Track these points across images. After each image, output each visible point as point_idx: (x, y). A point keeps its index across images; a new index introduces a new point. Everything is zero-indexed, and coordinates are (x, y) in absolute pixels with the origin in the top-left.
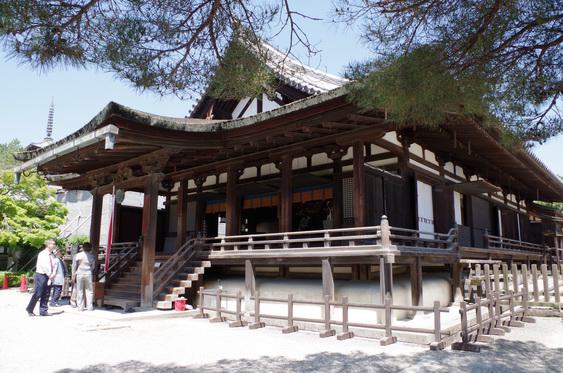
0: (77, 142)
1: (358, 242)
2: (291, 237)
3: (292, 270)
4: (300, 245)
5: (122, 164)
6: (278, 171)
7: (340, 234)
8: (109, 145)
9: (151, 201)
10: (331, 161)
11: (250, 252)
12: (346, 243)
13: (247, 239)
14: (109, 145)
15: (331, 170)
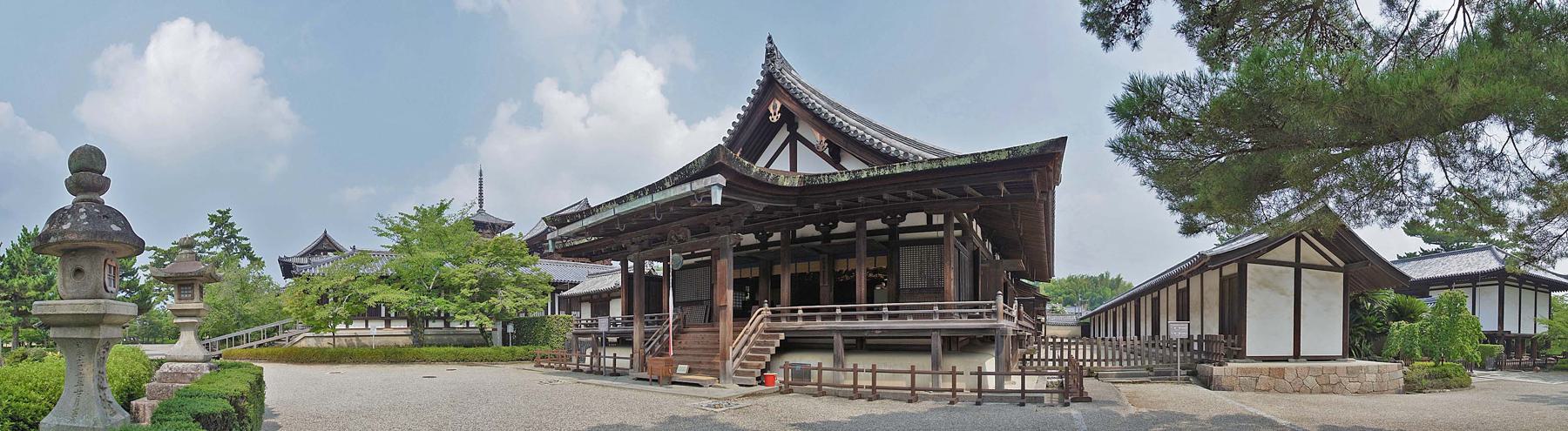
0: (659, 197)
1: (916, 316)
2: (890, 308)
3: (869, 341)
4: (814, 318)
5: (675, 224)
6: (818, 233)
7: (897, 308)
8: (717, 198)
9: (640, 266)
10: (818, 233)
11: (838, 324)
12: (904, 317)
13: (931, 307)
14: (717, 198)
15: (886, 237)
